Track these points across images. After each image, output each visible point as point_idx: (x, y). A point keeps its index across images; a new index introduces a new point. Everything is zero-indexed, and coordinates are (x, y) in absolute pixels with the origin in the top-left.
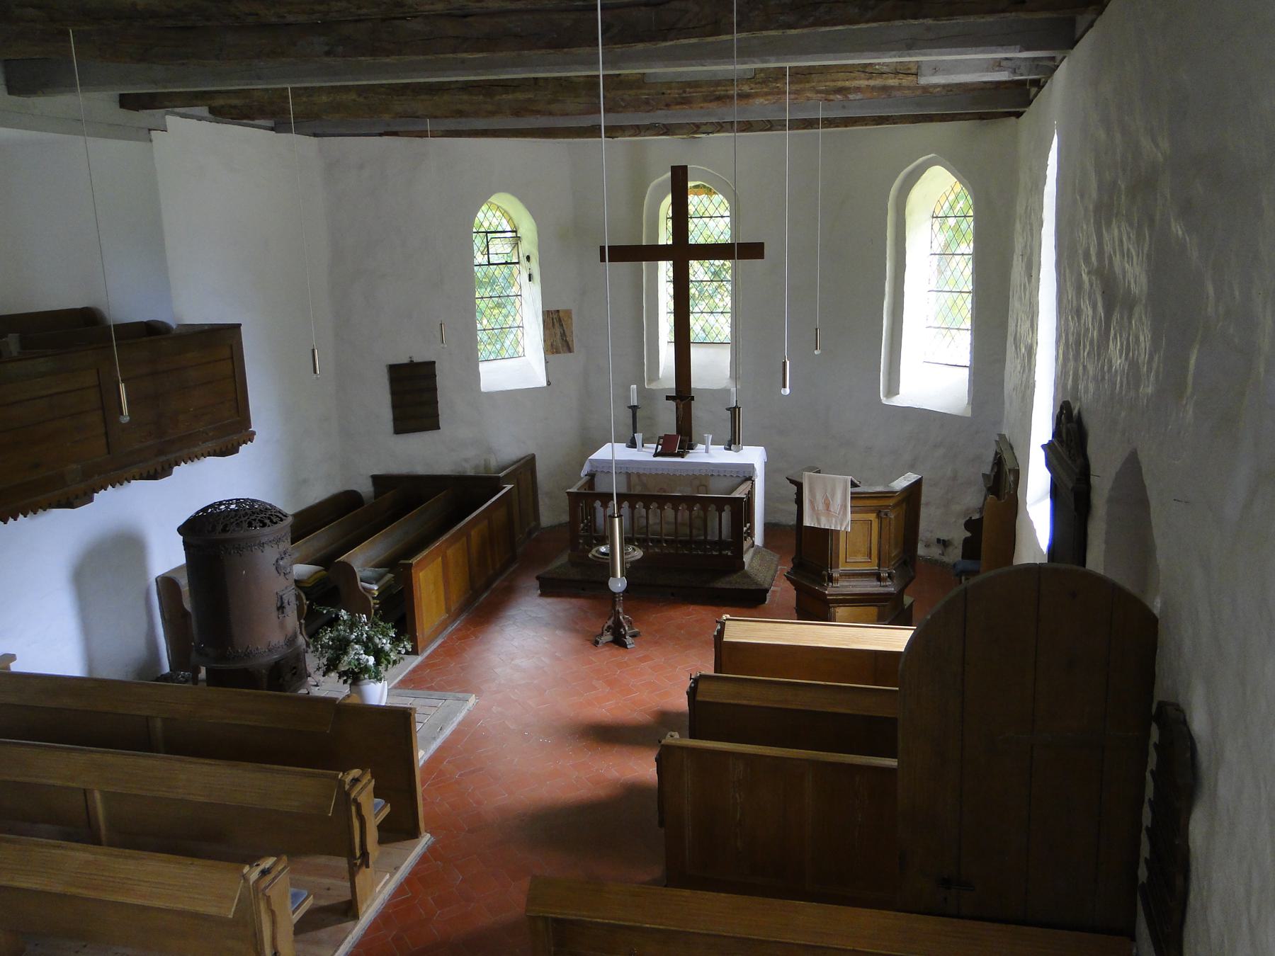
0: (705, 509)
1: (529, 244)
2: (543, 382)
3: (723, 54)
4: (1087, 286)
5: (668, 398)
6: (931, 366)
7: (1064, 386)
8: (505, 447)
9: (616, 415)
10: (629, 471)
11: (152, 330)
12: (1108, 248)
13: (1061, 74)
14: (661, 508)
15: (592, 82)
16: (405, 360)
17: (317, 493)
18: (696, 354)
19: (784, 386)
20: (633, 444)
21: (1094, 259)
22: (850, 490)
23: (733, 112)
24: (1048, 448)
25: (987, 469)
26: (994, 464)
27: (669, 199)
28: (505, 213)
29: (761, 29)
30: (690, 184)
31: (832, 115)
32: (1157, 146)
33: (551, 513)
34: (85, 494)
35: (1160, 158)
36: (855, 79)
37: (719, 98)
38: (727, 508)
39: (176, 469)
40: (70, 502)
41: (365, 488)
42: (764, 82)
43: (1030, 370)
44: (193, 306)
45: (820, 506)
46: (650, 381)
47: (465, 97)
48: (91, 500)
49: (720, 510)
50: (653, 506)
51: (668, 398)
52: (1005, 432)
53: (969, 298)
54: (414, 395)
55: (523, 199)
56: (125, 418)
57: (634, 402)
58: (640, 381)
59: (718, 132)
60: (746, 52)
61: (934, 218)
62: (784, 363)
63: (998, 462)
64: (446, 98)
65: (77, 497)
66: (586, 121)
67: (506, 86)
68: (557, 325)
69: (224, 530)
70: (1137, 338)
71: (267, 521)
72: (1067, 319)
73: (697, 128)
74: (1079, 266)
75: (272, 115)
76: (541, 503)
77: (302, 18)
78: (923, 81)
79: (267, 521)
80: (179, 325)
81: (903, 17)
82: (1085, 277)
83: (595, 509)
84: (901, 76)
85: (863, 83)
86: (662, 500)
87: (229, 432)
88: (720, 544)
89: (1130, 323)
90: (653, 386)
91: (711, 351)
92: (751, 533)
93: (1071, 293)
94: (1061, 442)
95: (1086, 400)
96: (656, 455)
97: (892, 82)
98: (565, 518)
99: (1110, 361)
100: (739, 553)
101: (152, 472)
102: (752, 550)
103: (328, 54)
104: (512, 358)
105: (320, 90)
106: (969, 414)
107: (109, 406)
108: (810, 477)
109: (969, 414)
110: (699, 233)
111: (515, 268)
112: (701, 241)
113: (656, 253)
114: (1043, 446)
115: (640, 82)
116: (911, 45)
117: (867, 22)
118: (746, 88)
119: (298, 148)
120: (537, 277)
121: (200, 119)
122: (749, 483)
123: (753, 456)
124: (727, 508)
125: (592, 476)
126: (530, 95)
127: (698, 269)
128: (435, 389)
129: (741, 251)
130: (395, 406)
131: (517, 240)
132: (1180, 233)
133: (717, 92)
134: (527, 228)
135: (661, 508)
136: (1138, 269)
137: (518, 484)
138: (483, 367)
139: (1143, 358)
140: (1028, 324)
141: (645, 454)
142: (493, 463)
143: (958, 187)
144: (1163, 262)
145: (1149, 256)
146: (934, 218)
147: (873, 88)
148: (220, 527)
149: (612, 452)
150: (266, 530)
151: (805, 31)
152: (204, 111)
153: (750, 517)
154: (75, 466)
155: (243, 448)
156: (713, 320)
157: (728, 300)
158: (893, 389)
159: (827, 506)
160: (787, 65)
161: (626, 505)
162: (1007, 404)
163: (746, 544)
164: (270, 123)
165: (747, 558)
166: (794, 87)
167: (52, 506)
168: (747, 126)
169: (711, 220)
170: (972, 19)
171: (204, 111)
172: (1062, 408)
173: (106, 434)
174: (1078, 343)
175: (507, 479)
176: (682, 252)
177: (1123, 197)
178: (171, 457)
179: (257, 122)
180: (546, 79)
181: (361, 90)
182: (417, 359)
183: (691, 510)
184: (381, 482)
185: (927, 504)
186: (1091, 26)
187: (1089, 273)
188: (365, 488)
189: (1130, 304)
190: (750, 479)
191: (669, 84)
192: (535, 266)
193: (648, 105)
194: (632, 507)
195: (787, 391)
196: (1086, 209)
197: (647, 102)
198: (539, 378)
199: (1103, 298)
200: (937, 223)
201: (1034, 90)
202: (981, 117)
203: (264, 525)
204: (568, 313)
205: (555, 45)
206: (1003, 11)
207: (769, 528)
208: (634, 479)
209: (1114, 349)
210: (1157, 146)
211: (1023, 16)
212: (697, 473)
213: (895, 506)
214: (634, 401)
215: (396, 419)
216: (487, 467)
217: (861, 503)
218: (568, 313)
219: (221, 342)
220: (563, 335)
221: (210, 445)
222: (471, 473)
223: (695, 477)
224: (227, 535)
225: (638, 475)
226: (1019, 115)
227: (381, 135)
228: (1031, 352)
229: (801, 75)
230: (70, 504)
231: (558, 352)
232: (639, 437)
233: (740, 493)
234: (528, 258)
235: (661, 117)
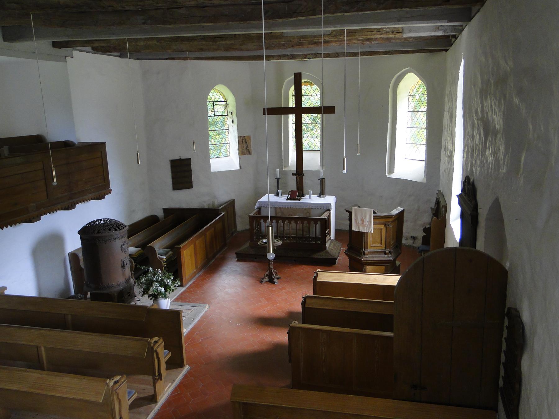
0: (309, 223)
1: (232, 107)
2: (238, 168)
3: (317, 24)
4: (476, 125)
5: (293, 174)
6: (408, 160)
7: (467, 169)
8: (222, 196)
9: (270, 182)
10: (276, 207)
11: (67, 145)
12: (486, 109)
13: (465, 33)
14: (290, 223)
15: (260, 36)
16: (178, 158)
17: (139, 216)
18: (305, 155)
19: (344, 169)
20: (277, 195)
21: (479, 113)
22: (372, 215)
23: (322, 49)
24: (459, 196)
25: (433, 205)
26: (436, 203)
27: (293, 87)
28: (221, 93)
29: (333, 13)
30: (303, 81)
31: (365, 50)
32: (507, 64)
33: (242, 225)
34: (37, 216)
36: (375, 34)
37: (315, 43)
38: (319, 223)
39: (77, 205)
40: (30, 220)
41: (160, 214)
43: (452, 162)
44: (85, 134)
45: (360, 222)
46: (285, 167)
47: (204, 43)
48: (40, 219)
49: (316, 224)
50: (286, 222)
51: (293, 174)
52: (441, 189)
53: (425, 131)
54: (182, 173)
55: (229, 87)
56: (55, 183)
57: (278, 176)
58: (280, 167)
59: (315, 58)
60: (327, 23)
61: (410, 96)
62: (344, 159)
63: (438, 202)
64: (196, 43)
65: (34, 218)
66: (257, 53)
67: (222, 38)
68: (244, 142)
69: (98, 232)
70: (499, 148)
71: (117, 229)
72: (468, 140)
73: (305, 56)
74: (473, 117)
75: (119, 50)
76: (237, 220)
77: (132, 8)
78: (405, 35)
79: (117, 229)
80: (78, 143)
81: (396, 8)
82: (476, 121)
83: (261, 223)
84: (395, 33)
85: (379, 36)
86: (290, 219)
87: (100, 189)
88: (316, 238)
89: (496, 141)
90: (286, 169)
91: (312, 154)
92: (329, 234)
93: (470, 129)
94: (465, 194)
95: (476, 175)
96: (288, 199)
97: (391, 36)
98: (248, 227)
99: (487, 158)
100: (324, 242)
101: (67, 207)
102: (330, 241)
103: (144, 23)
104: (225, 157)
105: (140, 39)
107: (48, 178)
110: (306, 102)
112: (307, 106)
113: (288, 111)
114: (457, 196)
115: (281, 36)
116: (399, 20)
117: (380, 9)
118: (327, 39)
119: (131, 65)
120: (235, 121)
121: (88, 52)
122: (328, 212)
123: (330, 200)
124: (319, 223)
125: (259, 209)
126: (233, 42)
127: (306, 118)
128: (191, 171)
129: (325, 110)
130: (173, 178)
131: (227, 105)
132: (517, 102)
133: (315, 41)
134: (231, 100)
135: (290, 223)
136: (499, 118)
137: (227, 212)
138: (212, 161)
139: (501, 157)
140: (451, 142)
141: (283, 199)
142: (216, 203)
143: (420, 82)
144: (510, 115)
145: (504, 112)
146: (410, 96)
147: (383, 39)
148: (96, 231)
149: (268, 198)
150: (117, 232)
151: (353, 13)
152: (89, 49)
153: (329, 227)
155: (106, 196)
156: (313, 140)
158: (392, 171)
159: (363, 222)
160: (345, 28)
161: (274, 221)
162: (441, 177)
163: (327, 239)
164: (118, 54)
165: (327, 245)
166: (348, 38)
167: (23, 222)
168: (328, 55)
169: (312, 96)
170: (426, 8)
171: (89, 49)
172: (465, 179)
173: (47, 190)
174: (473, 150)
175: (222, 210)
176: (299, 110)
178: (75, 200)
179: (113, 53)
180: (239, 35)
182: (183, 157)
184: (167, 211)
185: (407, 221)
186: (478, 11)
187: (477, 120)
188: (160, 214)
189: (495, 133)
190: (329, 210)
192: (234, 117)
193: (284, 46)
194: (277, 222)
195: (345, 171)
196: (476, 92)
197: (284, 45)
198: (236, 166)
200: (411, 98)
201: (453, 40)
202: (430, 51)
203: (116, 230)
204: (249, 137)
205: (244, 20)
206: (440, 5)
207: (337, 231)
208: (278, 210)
209: (489, 153)
210: (507, 64)
211: (448, 7)
212: (306, 207)
213: (393, 222)
214: (278, 176)
215: (173, 184)
216: (213, 205)
217: (377, 220)
218: (249, 137)
219: (97, 150)
220: (247, 147)
221: (92, 195)
222: (206, 207)
223: (305, 209)
224: (100, 235)
225: (280, 208)
226: (447, 50)
227: (167, 59)
229: (351, 33)
230: (31, 221)
232: (280, 192)
233: (324, 216)
234: (232, 113)
235: (290, 51)
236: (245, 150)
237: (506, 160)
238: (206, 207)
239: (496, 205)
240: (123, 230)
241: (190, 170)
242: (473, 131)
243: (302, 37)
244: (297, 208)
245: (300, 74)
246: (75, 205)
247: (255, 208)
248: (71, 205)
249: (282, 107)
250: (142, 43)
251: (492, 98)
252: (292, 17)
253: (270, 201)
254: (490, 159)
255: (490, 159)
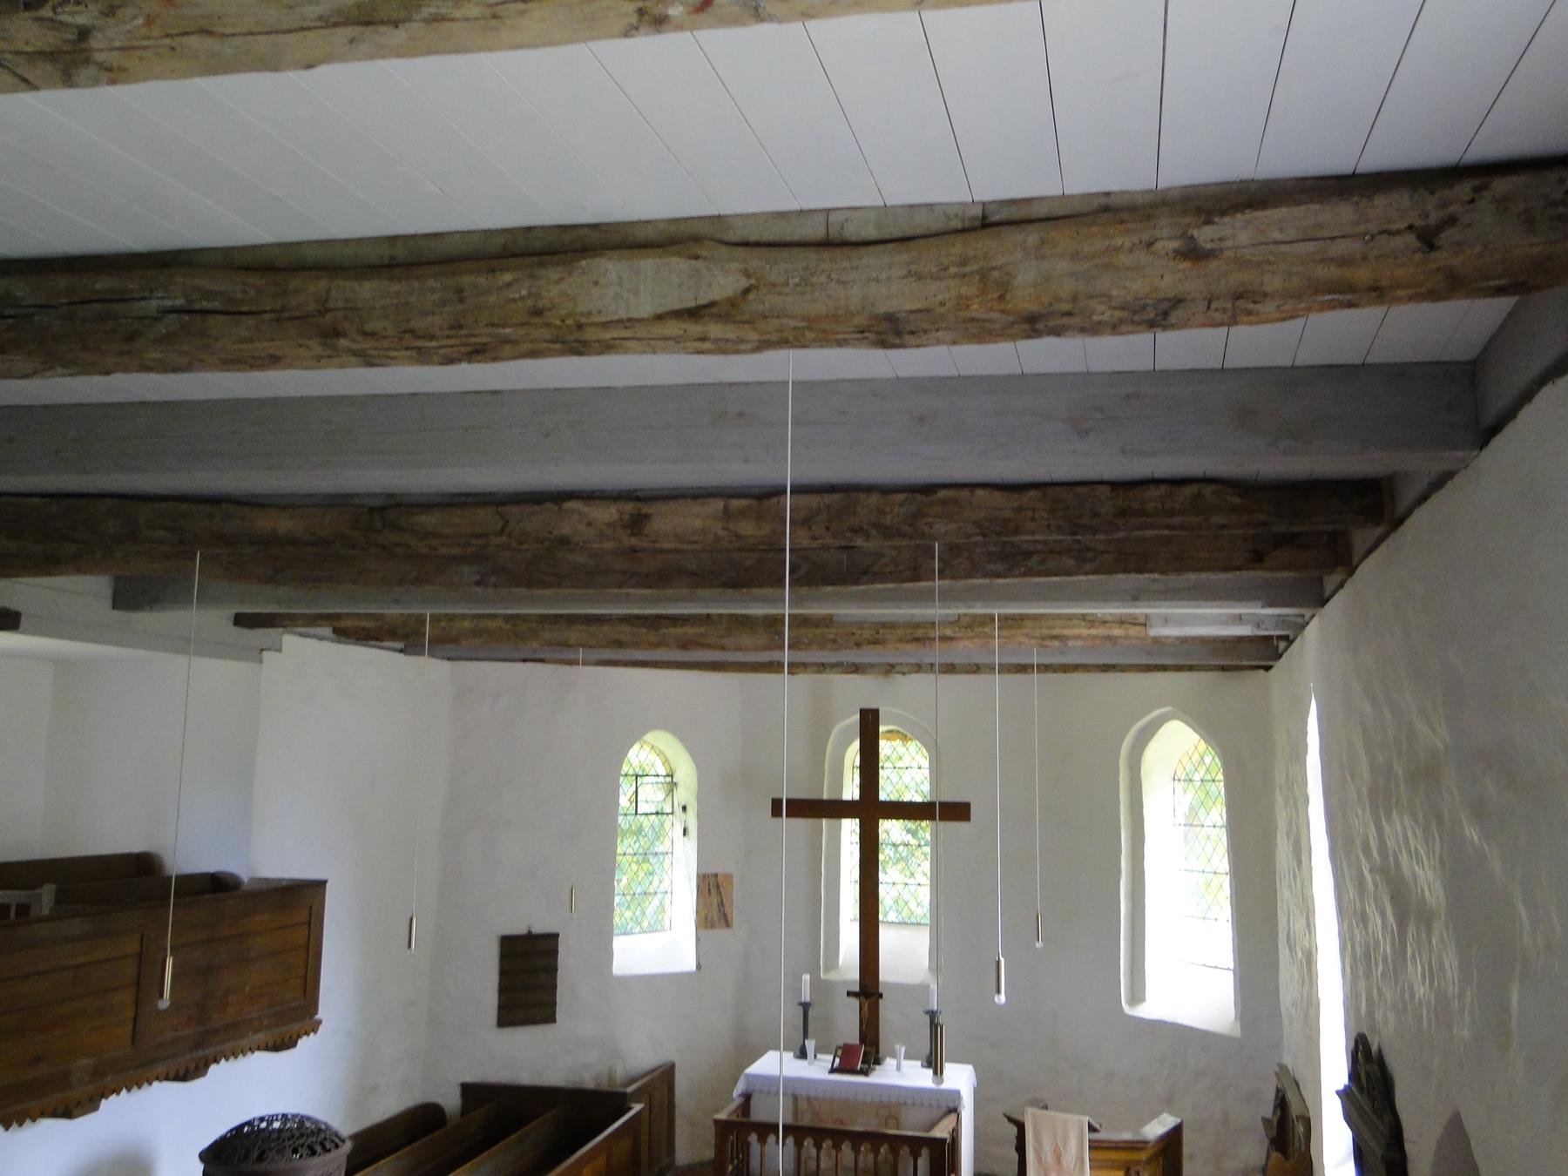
0: (895, 1152)
1: (687, 791)
3: (926, 598)
4: (1370, 887)
5: (849, 994)
6: (1186, 972)
7: (1357, 1011)
8: (636, 1050)
9: (786, 1017)
10: (799, 1093)
11: (218, 885)
12: (1391, 844)
13: (1312, 631)
14: (837, 1147)
15: (774, 623)
17: (388, 1105)
18: (886, 937)
19: (999, 991)
20: (802, 1054)
21: (1375, 853)
22: (1087, 1135)
23: (936, 654)
24: (1345, 1095)
25: (1267, 1109)
26: (1276, 1107)
27: (856, 746)
28: (661, 754)
29: (966, 577)
30: (882, 729)
31: (1046, 661)
32: (1434, 730)
33: (691, 1143)
34: (91, 1099)
35: (1440, 746)
36: (1073, 627)
37: (917, 640)
38: (925, 1152)
40: (67, 1112)
41: (450, 1100)
42: (969, 626)
43: (1311, 982)
44: (270, 858)
45: (1049, 1158)
46: (827, 969)
47: (627, 629)
48: (95, 1108)
49: (916, 1155)
50: (827, 1144)
51: (849, 994)
52: (1288, 1061)
53: (1228, 878)
54: (529, 976)
55: (684, 739)
56: (164, 1003)
58: (814, 970)
60: (947, 597)
61: (1177, 782)
63: (1281, 1103)
64: (605, 629)
65: (79, 1104)
66: (765, 657)
67: (675, 620)
69: (260, 1158)
70: (1441, 963)
71: (318, 1149)
72: (1350, 924)
73: (890, 669)
74: (1358, 860)
75: (405, 637)
76: (678, 1131)
77: (456, 551)
78: (1154, 632)
79: (318, 1149)
80: (252, 879)
81: (1126, 571)
82: (1366, 873)
83: (748, 1145)
85: (1084, 632)
86: (839, 1136)
87: (286, 1017)
89: (1430, 943)
90: (832, 976)
91: (906, 933)
93: (1352, 893)
94: (1361, 1089)
95: (1385, 1037)
96: (832, 1071)
97: (1117, 632)
98: (709, 1154)
99: (1411, 989)
103: (478, 583)
104: (653, 933)
105: (463, 617)
106: (1237, 1033)
107: (146, 983)
108: (1035, 1117)
109: (1237, 1033)
111: (668, 820)
112: (894, 798)
113: (838, 809)
114: (1338, 1093)
115: (828, 621)
116: (1136, 597)
117: (1086, 574)
118: (949, 632)
119: (430, 671)
120: (693, 831)
121: (321, 639)
122: (953, 1117)
123: (960, 1078)
124: (925, 1152)
125: (747, 1097)
126: (702, 630)
127: (891, 830)
128: (555, 969)
129: (943, 811)
130: (503, 990)
131: (672, 786)
133: (918, 634)
134: (686, 772)
135: (837, 1147)
136: (1430, 875)
137: (650, 1105)
138: (619, 943)
139: (1452, 990)
140: (1303, 922)
141: (817, 1069)
142: (620, 1073)
143: (1203, 746)
144: (1460, 869)
145: (1442, 862)
146: (1177, 782)
147: (1095, 637)
148: (255, 1155)
149: (773, 1064)
150: (316, 1160)
151: (1016, 580)
152: (327, 631)
154: (86, 1061)
155: (303, 1042)
156: (908, 881)
157: (926, 866)
158: (1137, 996)
159: (1058, 1157)
160: (996, 612)
161: (790, 1140)
162: (1286, 1022)
164: (400, 645)
166: (1005, 633)
167: (43, 1114)
168: (950, 669)
169: (907, 772)
170: (1204, 575)
171: (327, 631)
172: (1356, 1042)
173: (135, 1020)
175: (637, 1096)
176: (871, 809)
177: (1402, 787)
179: (386, 644)
180: (720, 616)
181: (507, 618)
183: (876, 1153)
184: (472, 1092)
185: (1191, 1157)
186: (1341, 586)
187: (1371, 870)
188: (450, 1100)
189: (1426, 918)
190: (954, 1110)
191: (860, 625)
192: (692, 819)
193: (835, 644)
194: (799, 1145)
195: (1002, 999)
196: (1359, 792)
197: (834, 641)
198: (686, 961)
199: (1393, 906)
200: (1179, 786)
201: (1282, 645)
202: (1223, 668)
203: (313, 1153)
204: (729, 877)
205: (735, 584)
206: (1239, 569)
208: (803, 1105)
209: (1415, 971)
210: (1434, 730)
211: (1260, 573)
212: (885, 1099)
213: (1149, 1161)
214: (806, 996)
216: (611, 1078)
218: (729, 877)
219: (299, 901)
221: (260, 1037)
222: (590, 1085)
223: (883, 1105)
224: (261, 1167)
225: (809, 1099)
226: (1268, 668)
227: (525, 661)
228: (1309, 959)
229: (1010, 622)
230: (68, 1114)
231: (713, 926)
232: (810, 1045)
233: (941, 1132)
234: (684, 808)
235: (850, 656)
236: (715, 914)
237: (1468, 1001)
238: (590, 1084)
239: (1456, 1130)
240: (335, 1153)
241: (553, 970)
242: (1362, 899)
243: (883, 625)
244: (860, 1098)
245: (876, 713)
246: (207, 1066)
247: (736, 1093)
248: (197, 1067)
249: (825, 797)
250: (467, 624)
251: (1406, 818)
252: (857, 583)
253: (777, 1054)
254: (1421, 991)
255: (1421, 991)
